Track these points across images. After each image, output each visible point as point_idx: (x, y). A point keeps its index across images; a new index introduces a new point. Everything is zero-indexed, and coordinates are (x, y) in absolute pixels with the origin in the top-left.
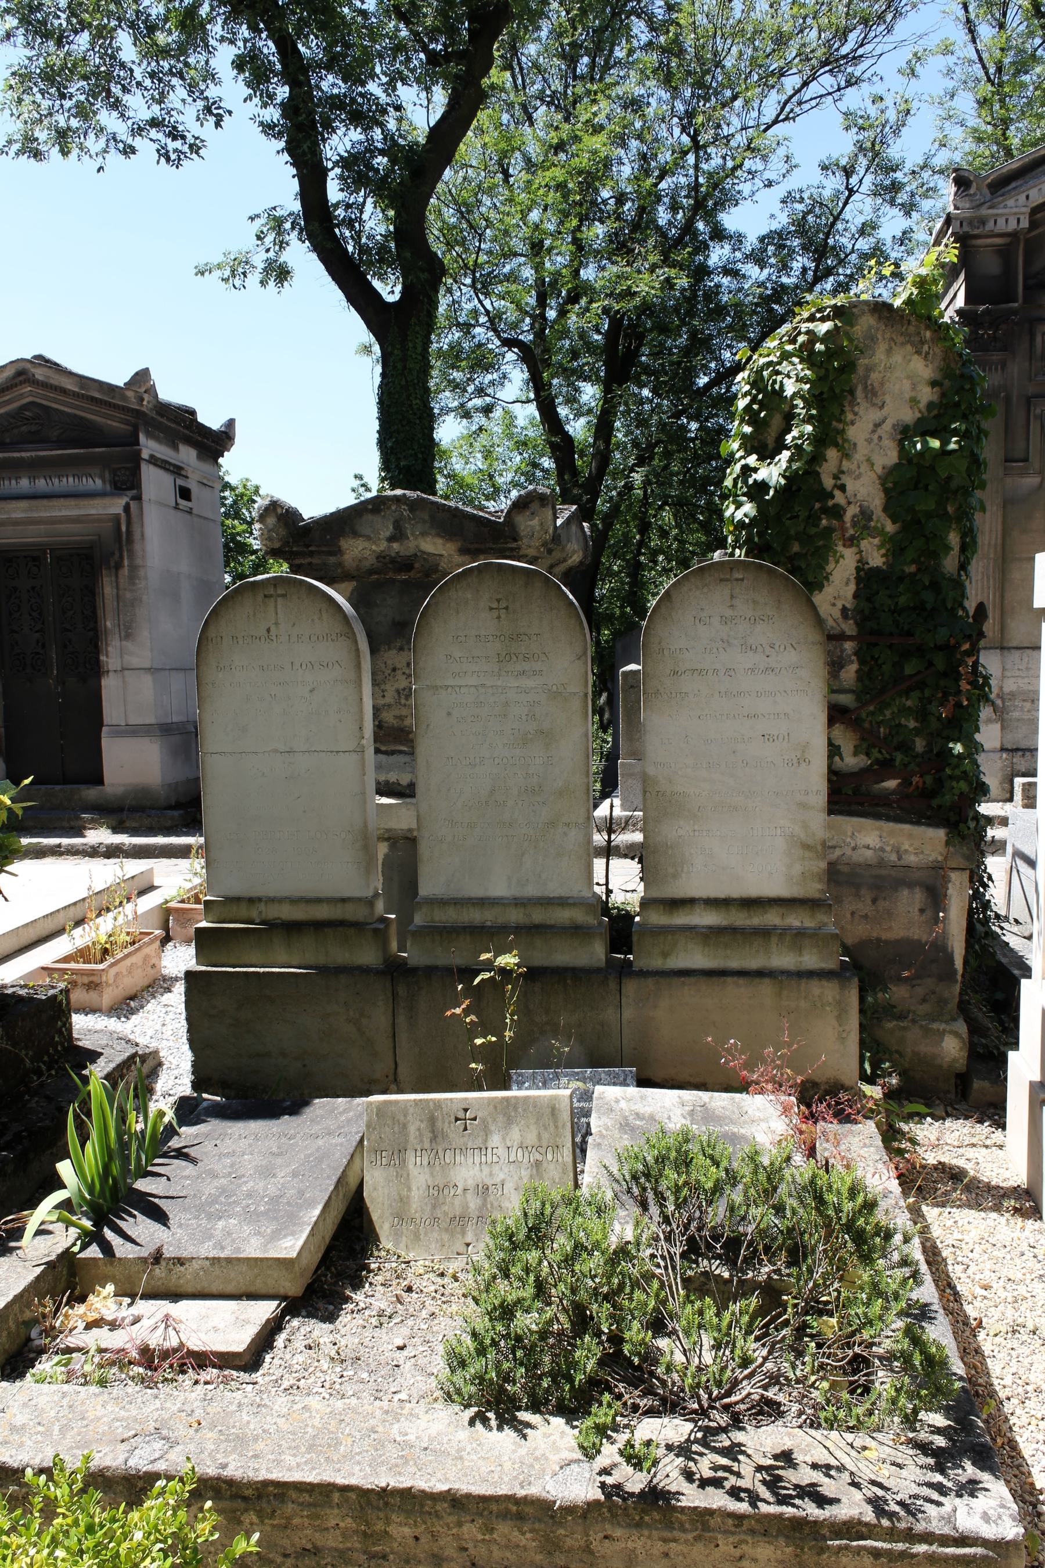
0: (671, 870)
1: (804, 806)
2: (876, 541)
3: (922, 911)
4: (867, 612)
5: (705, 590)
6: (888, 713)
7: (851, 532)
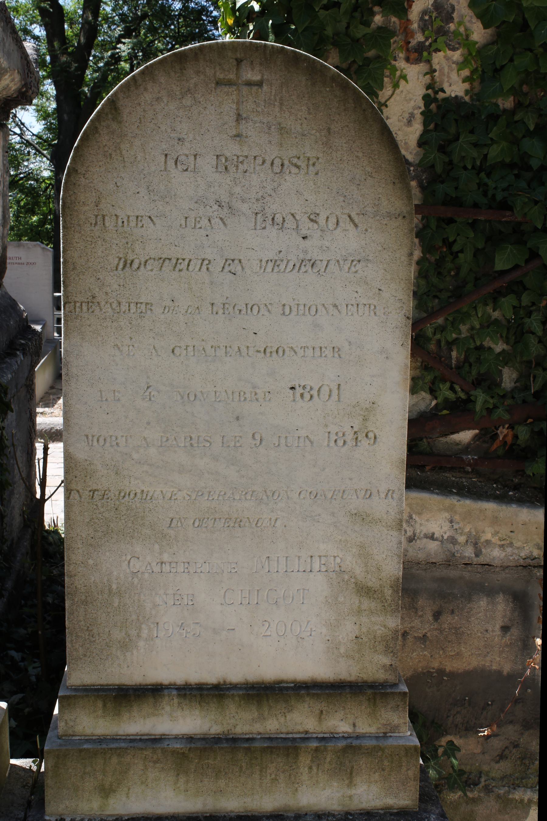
0: (117, 635)
1: (362, 518)
2: (457, 55)
3: (505, 629)
4: (439, 169)
5: (188, 101)
6: (464, 328)
7: (419, 37)
